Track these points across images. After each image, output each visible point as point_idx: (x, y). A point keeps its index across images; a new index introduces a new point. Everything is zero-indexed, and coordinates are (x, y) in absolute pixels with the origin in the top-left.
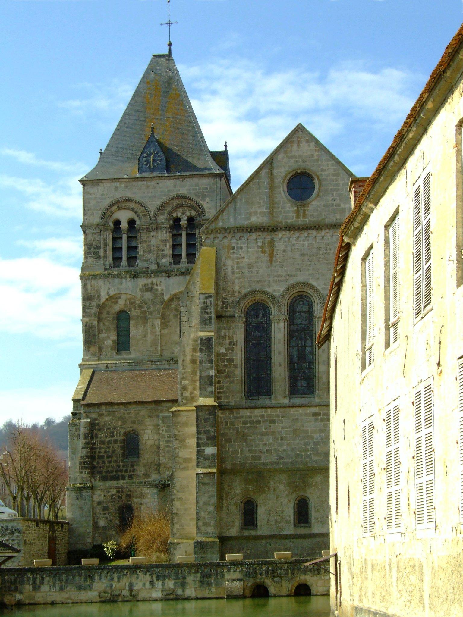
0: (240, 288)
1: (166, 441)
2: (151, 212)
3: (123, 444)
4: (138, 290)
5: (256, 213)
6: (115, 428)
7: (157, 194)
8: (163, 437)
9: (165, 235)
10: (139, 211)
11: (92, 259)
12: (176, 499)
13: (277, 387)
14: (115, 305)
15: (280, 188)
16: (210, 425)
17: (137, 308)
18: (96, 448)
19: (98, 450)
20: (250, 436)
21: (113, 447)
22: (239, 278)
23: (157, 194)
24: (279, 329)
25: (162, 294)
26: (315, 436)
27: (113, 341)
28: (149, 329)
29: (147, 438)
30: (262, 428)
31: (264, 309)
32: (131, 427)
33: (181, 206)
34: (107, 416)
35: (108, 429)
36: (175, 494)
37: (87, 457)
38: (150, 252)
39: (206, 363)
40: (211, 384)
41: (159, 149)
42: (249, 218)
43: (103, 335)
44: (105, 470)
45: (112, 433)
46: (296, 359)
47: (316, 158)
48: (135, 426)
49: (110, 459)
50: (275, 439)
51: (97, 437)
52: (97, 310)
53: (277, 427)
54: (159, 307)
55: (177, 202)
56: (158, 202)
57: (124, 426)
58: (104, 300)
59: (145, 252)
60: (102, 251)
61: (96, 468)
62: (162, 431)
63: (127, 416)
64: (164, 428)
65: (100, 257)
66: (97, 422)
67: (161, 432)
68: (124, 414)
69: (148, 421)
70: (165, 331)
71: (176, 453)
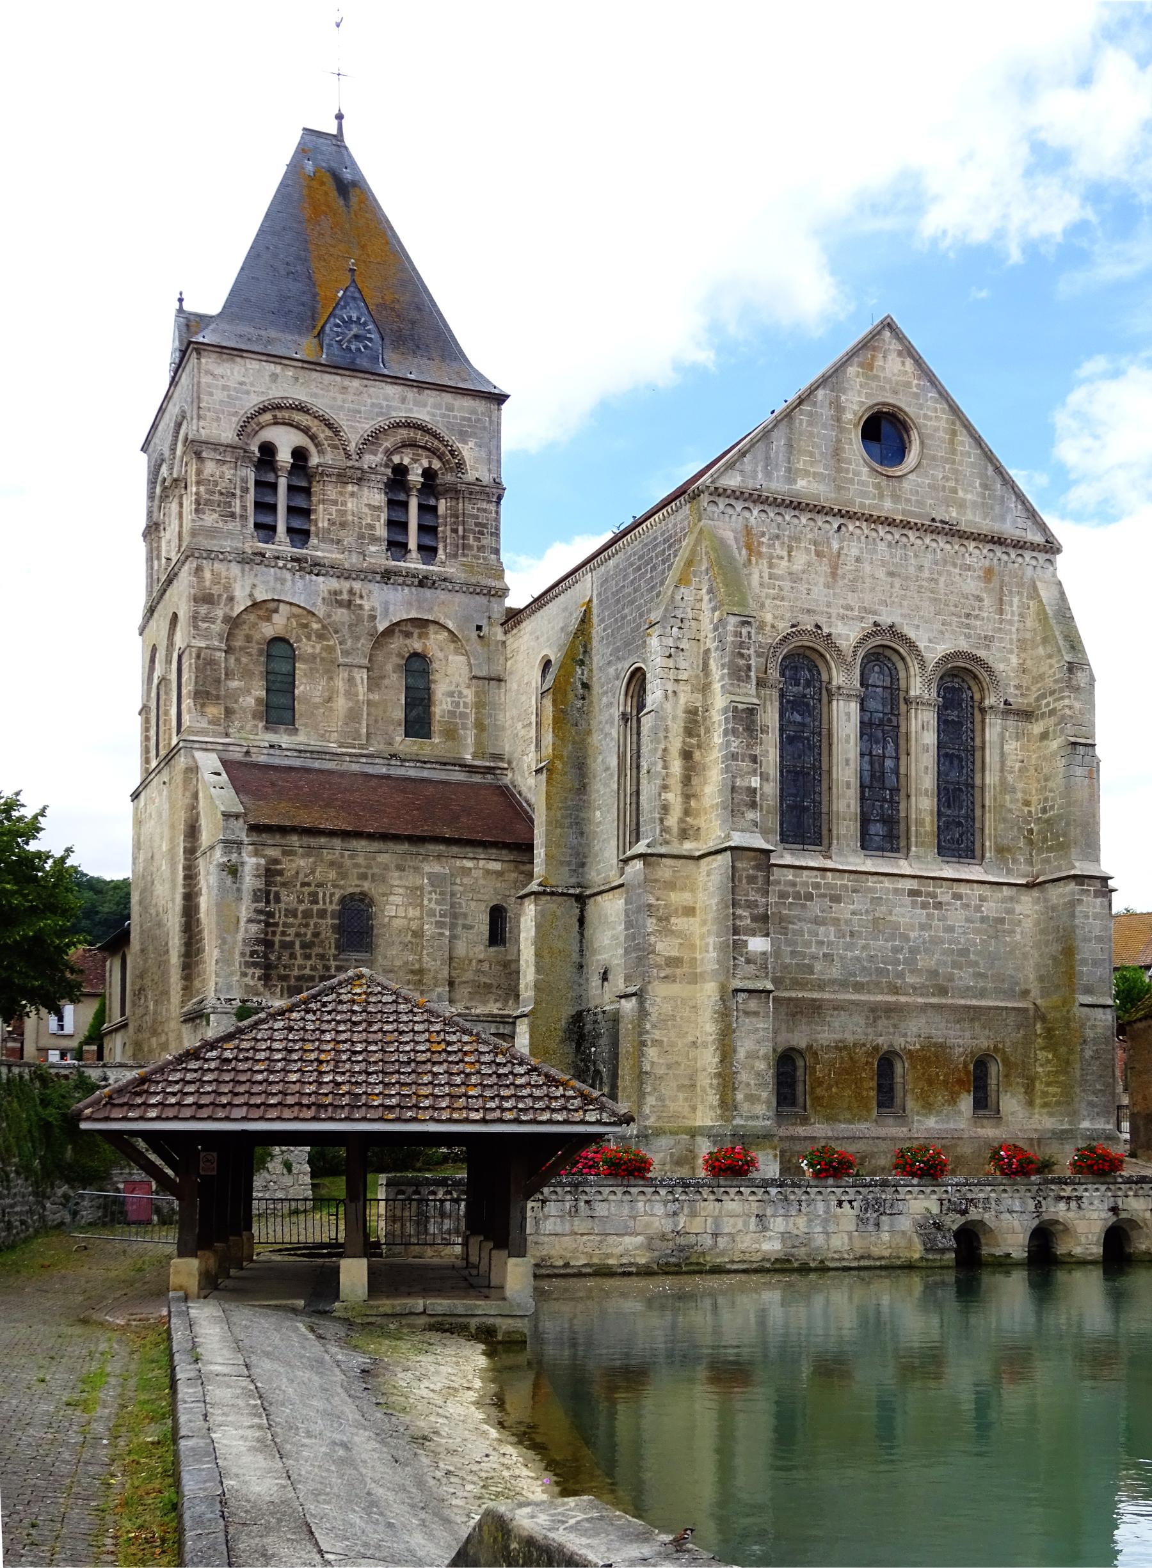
0: (775, 617)
1: (437, 922)
2: (350, 442)
3: (337, 922)
4: (320, 600)
5: (807, 473)
6: (319, 885)
7: (363, 408)
8: (432, 913)
9: (377, 496)
10: (322, 436)
11: (216, 516)
12: (649, 1043)
13: (843, 831)
14: (265, 624)
15: (850, 433)
16: (758, 890)
17: (314, 638)
18: (276, 925)
19: (281, 929)
20: (793, 923)
21: (316, 924)
22: (774, 599)
23: (363, 408)
24: (848, 714)
25: (373, 618)
26: (912, 935)
27: (258, 700)
28: (340, 684)
29: (393, 914)
30: (816, 908)
31: (810, 671)
32: (357, 886)
33: (412, 444)
34: (303, 856)
35: (303, 885)
36: (647, 1032)
37: (259, 941)
38: (343, 525)
39: (743, 761)
40: (753, 805)
41: (369, 319)
42: (791, 480)
43: (234, 684)
44: (296, 972)
45: (315, 894)
46: (867, 782)
47: (915, 390)
48: (366, 886)
49: (308, 951)
50: (840, 934)
51: (278, 900)
52: (226, 628)
53: (843, 910)
54: (365, 644)
55: (404, 433)
56: (367, 426)
57: (342, 882)
58: (242, 608)
59: (334, 524)
60: (238, 502)
61: (276, 967)
62: (430, 900)
63: (348, 862)
64: (434, 896)
65: (233, 515)
66: (278, 867)
67: (426, 902)
68: (342, 856)
69: (394, 878)
70: (375, 697)
71: (650, 945)
